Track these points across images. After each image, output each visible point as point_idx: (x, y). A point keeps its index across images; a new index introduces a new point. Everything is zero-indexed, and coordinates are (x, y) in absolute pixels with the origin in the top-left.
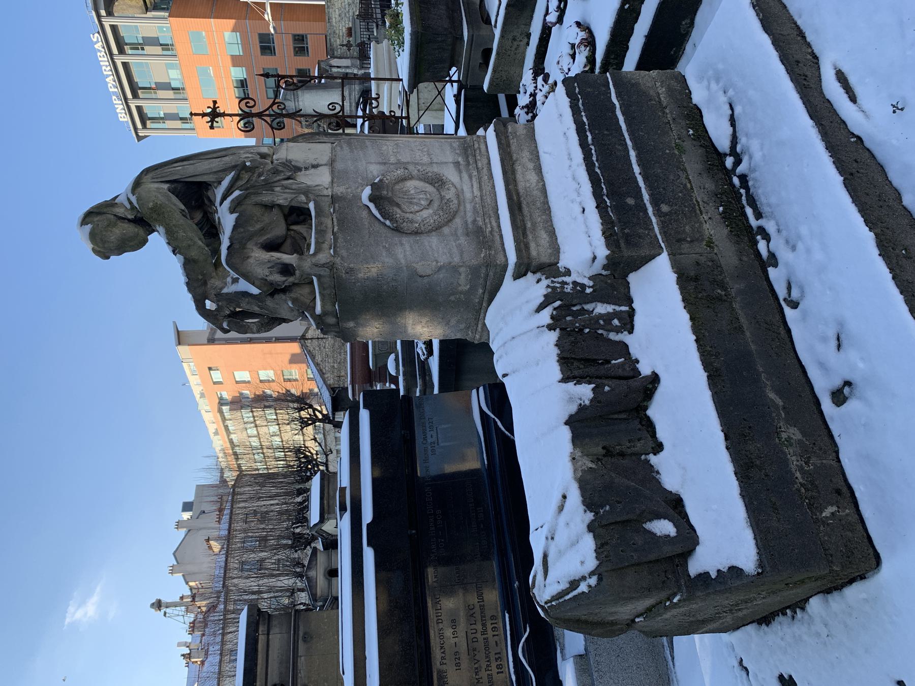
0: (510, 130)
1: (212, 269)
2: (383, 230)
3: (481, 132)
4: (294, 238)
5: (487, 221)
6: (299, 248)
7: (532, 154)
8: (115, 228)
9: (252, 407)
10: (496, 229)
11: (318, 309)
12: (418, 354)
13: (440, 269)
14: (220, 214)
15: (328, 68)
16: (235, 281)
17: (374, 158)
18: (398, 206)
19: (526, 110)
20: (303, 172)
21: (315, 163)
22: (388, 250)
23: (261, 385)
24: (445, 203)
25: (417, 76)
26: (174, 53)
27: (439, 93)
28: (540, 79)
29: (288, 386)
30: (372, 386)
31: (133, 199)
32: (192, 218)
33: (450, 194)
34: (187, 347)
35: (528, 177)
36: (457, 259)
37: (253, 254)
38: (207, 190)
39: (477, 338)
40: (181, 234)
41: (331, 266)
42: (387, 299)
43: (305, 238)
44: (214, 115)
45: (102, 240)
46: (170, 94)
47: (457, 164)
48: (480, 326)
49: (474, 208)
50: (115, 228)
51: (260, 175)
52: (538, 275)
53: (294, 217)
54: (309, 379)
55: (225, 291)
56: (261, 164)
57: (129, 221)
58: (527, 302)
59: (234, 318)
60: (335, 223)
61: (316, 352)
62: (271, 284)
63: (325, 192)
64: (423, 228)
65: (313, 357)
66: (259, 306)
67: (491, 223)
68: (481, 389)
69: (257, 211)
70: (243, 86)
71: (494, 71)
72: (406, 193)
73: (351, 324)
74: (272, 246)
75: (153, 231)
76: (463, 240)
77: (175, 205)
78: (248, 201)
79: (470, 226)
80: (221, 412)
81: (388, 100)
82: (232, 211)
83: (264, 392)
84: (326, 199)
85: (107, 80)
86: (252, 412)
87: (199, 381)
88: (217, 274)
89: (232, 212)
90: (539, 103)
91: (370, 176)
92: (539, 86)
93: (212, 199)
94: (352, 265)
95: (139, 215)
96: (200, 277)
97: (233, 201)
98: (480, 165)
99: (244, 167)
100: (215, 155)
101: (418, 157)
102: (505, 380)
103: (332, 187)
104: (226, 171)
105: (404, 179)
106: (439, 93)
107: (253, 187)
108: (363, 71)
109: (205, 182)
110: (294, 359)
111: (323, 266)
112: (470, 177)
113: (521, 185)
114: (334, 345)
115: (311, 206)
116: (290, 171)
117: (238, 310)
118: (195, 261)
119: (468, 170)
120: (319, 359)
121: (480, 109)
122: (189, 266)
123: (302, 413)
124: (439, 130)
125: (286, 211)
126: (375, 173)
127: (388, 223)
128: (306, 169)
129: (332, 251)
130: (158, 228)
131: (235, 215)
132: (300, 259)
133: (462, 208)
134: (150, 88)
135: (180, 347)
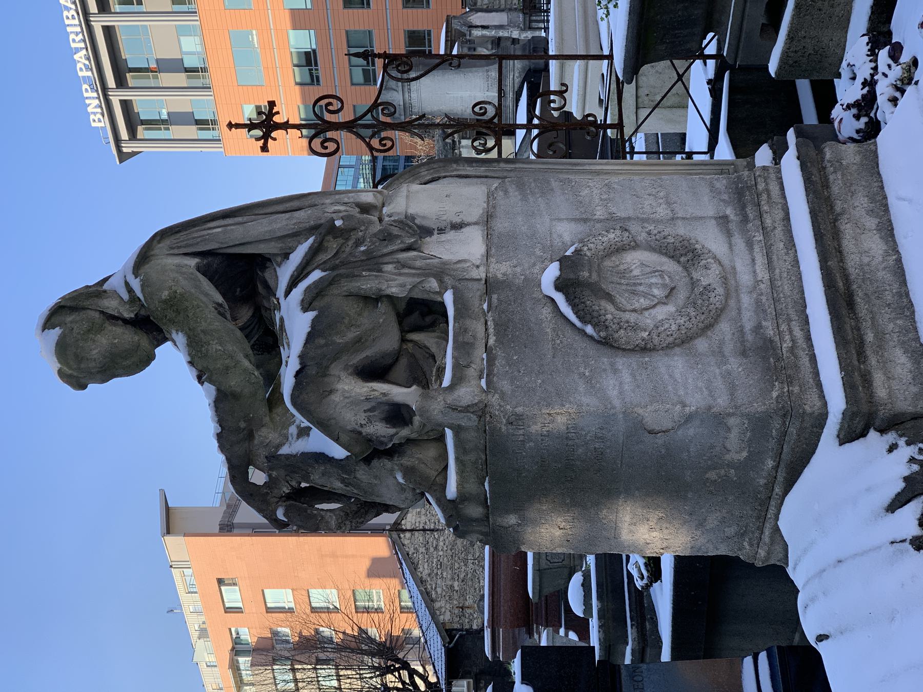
0: (828, 156)
1: (264, 409)
2: (581, 344)
3: (763, 156)
4: (413, 356)
5: (784, 327)
6: (422, 374)
7: (872, 200)
8: (100, 335)
9: (293, 661)
10: (801, 342)
11: (452, 490)
12: (630, 576)
13: (689, 418)
14: (284, 312)
15: (464, 29)
16: (304, 432)
17: (566, 210)
18: (609, 298)
19: (854, 111)
20: (435, 236)
21: (457, 220)
22: (589, 381)
23: (313, 617)
24: (699, 295)
25: (641, 51)
26: (192, 7)
27: (680, 77)
28: (883, 54)
29: (364, 620)
30: (530, 634)
31: (136, 284)
32: (234, 319)
33: (709, 277)
34: (180, 540)
35: (866, 245)
36: (722, 401)
37: (340, 386)
38: (264, 268)
39: (761, 556)
40: (215, 346)
41: (481, 411)
42: (586, 474)
43: (433, 357)
44: (266, 125)
45: (76, 356)
46: (180, 79)
47: (723, 220)
48: (767, 532)
49: (758, 303)
50: (100, 335)
51: (358, 243)
52: (891, 437)
53: (415, 318)
54: (403, 610)
55: (285, 450)
56: (362, 222)
57: (126, 322)
58: (868, 490)
59: (286, 495)
60: (491, 330)
61: (420, 558)
62: (369, 440)
63: (475, 274)
64: (656, 341)
65: (414, 567)
66: (343, 481)
67: (791, 331)
68: (763, 657)
69: (351, 308)
70: (308, 63)
71: (790, 38)
72: (623, 274)
73: (512, 520)
74: (373, 372)
75: (165, 340)
76: (734, 364)
77: (207, 295)
78: (335, 290)
79: (750, 337)
80: (235, 667)
81: (581, 91)
82: (306, 306)
83: (317, 632)
84: (475, 285)
85: (76, 57)
86: (293, 670)
87: (199, 606)
88: (272, 419)
89: (305, 309)
90: (882, 100)
91: (557, 242)
92: (882, 68)
93: (271, 283)
94: (520, 410)
95: (143, 312)
96: (243, 425)
97: (308, 289)
98: (768, 222)
99: (331, 230)
100: (280, 208)
101: (647, 209)
102: (821, 648)
103: (487, 265)
104: (298, 235)
105: (620, 249)
106: (680, 77)
107: (343, 264)
108: (529, 35)
109: (260, 255)
110: (376, 570)
111: (467, 409)
112: (750, 244)
113: (852, 261)
114: (454, 545)
115: (448, 298)
116: (413, 235)
117: (303, 485)
118: (235, 396)
119: (744, 232)
120: (424, 570)
121: (759, 110)
122: (223, 403)
123: (389, 677)
124: (676, 143)
125: (402, 306)
126: (567, 238)
127: (589, 329)
128: (441, 231)
129: (483, 383)
130: (174, 335)
131: (311, 315)
132: (425, 397)
133: (732, 303)
134: (147, 70)
135: (168, 539)
